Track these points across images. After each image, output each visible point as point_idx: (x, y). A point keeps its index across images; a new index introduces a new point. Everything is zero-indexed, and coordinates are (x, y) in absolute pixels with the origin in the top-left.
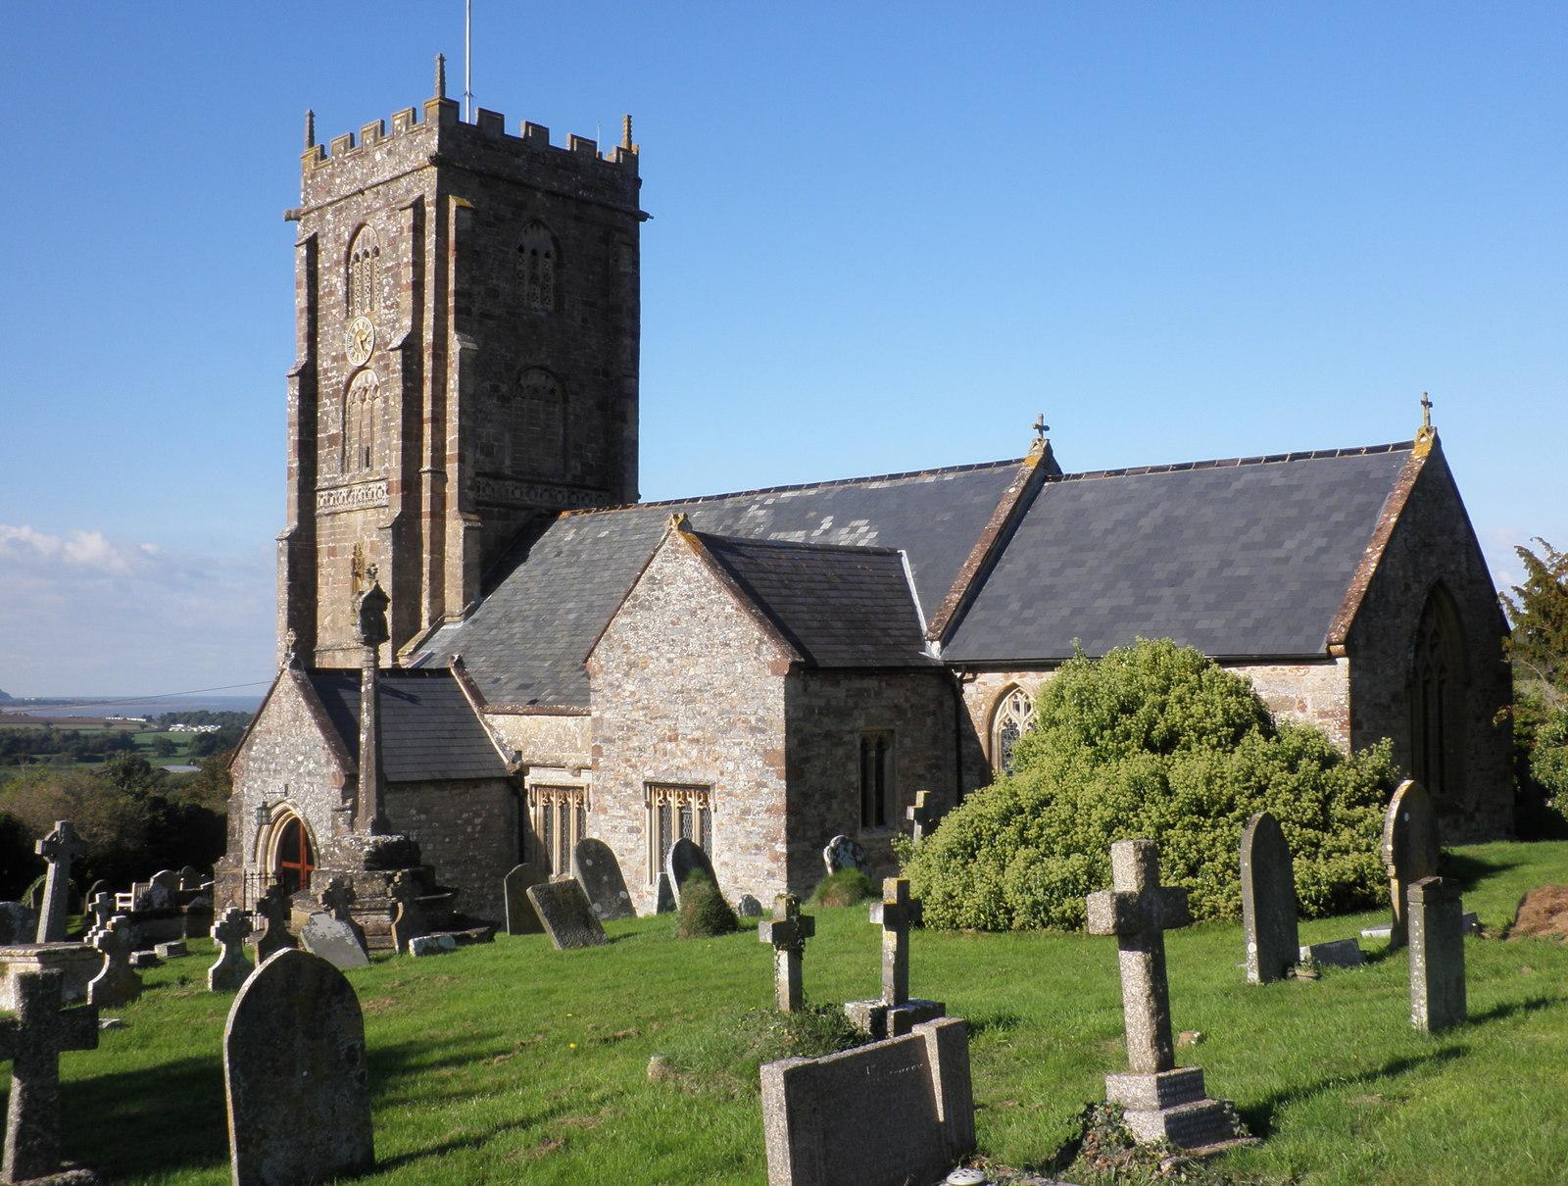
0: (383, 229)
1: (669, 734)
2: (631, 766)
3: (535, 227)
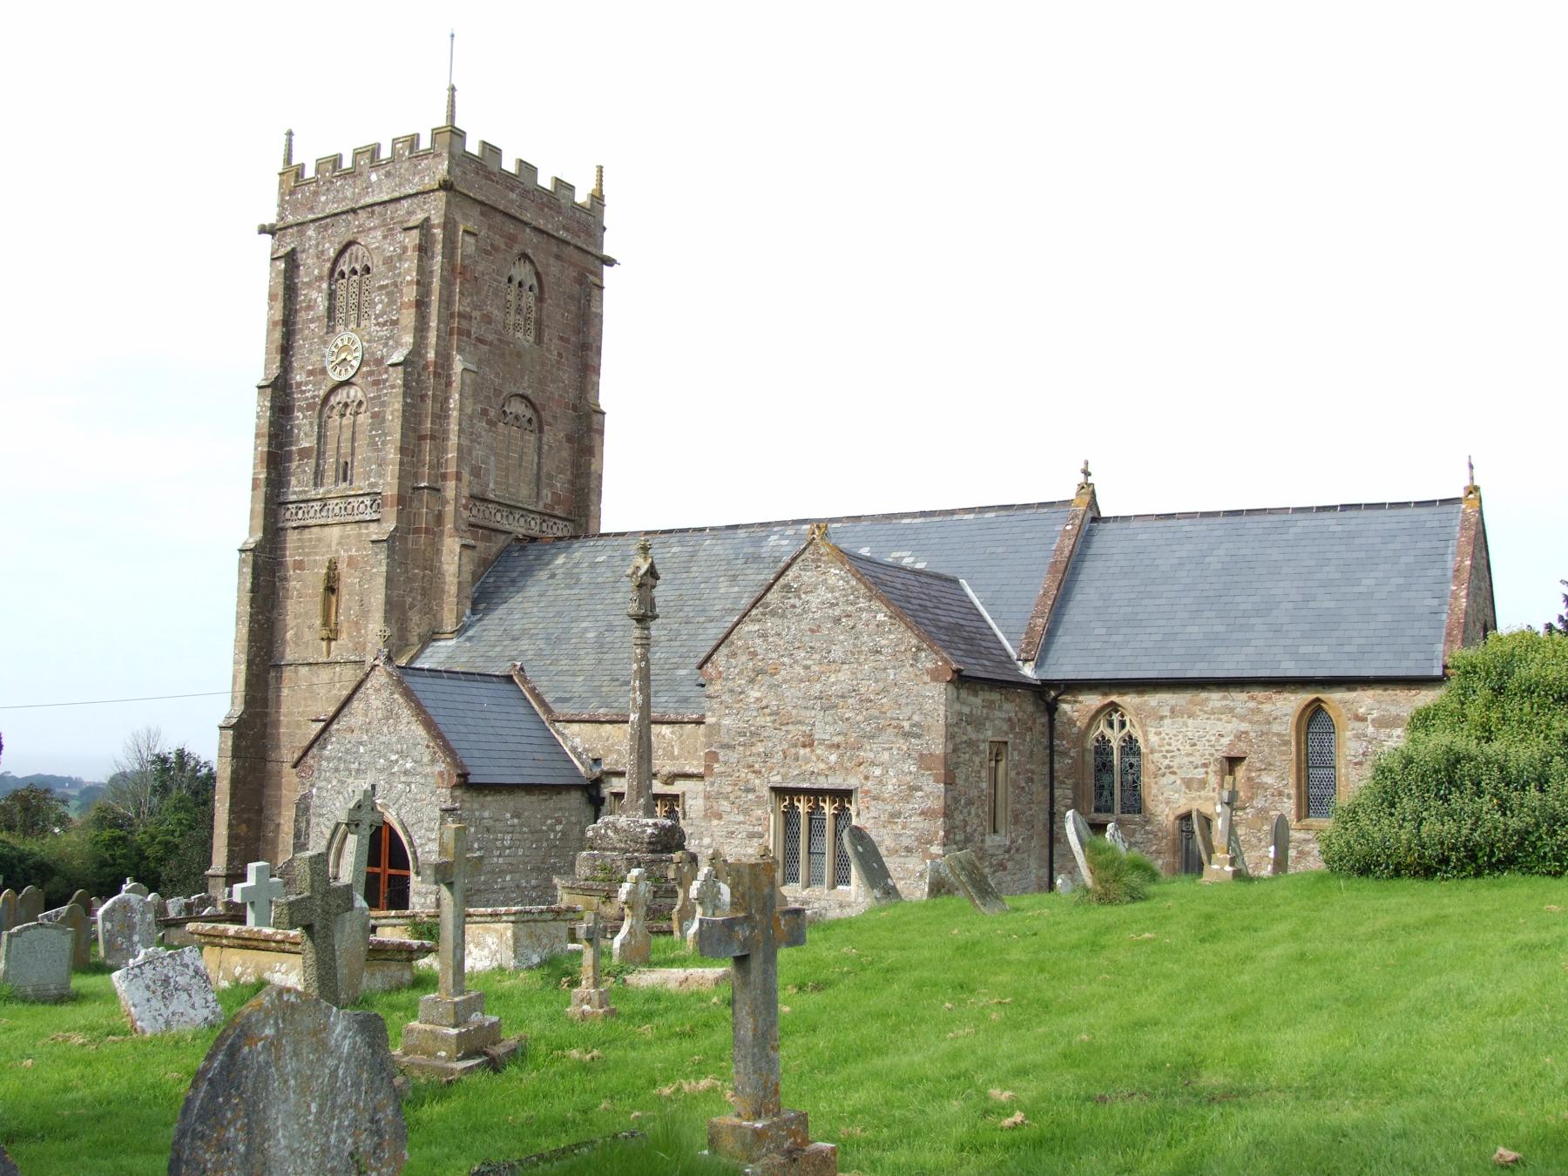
0: (377, 248)
1: (801, 739)
2: (754, 772)
3: (522, 261)
